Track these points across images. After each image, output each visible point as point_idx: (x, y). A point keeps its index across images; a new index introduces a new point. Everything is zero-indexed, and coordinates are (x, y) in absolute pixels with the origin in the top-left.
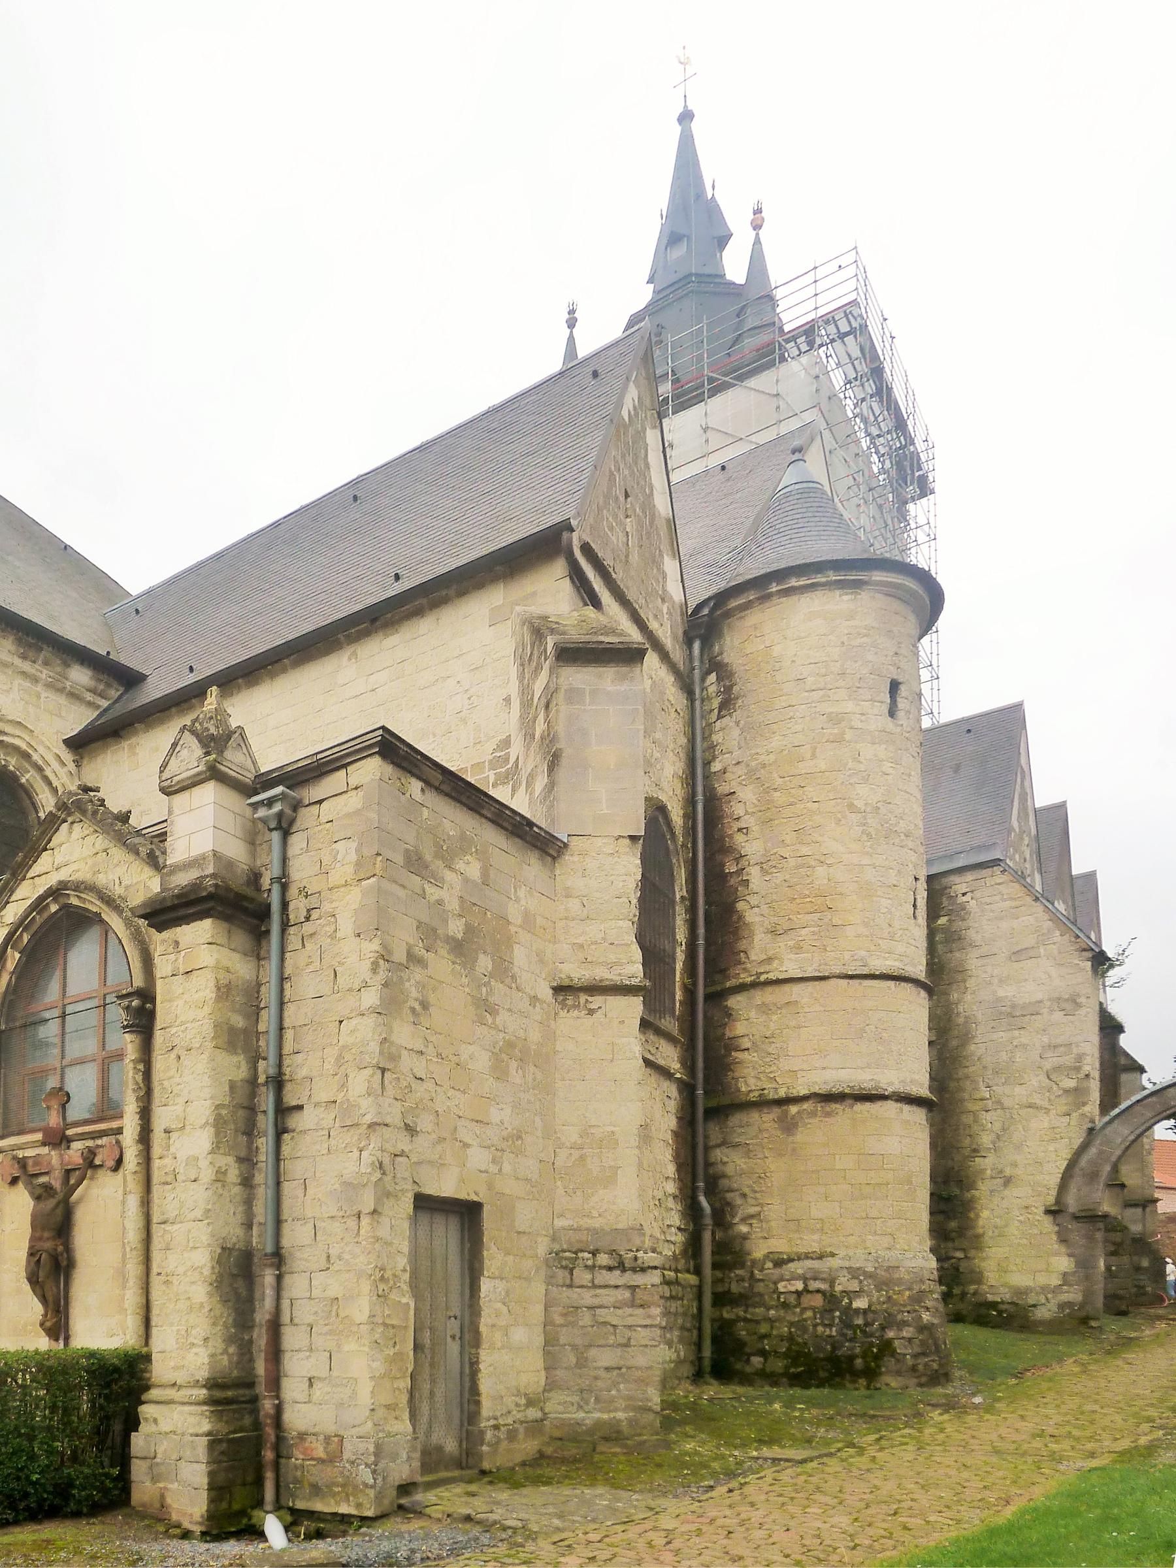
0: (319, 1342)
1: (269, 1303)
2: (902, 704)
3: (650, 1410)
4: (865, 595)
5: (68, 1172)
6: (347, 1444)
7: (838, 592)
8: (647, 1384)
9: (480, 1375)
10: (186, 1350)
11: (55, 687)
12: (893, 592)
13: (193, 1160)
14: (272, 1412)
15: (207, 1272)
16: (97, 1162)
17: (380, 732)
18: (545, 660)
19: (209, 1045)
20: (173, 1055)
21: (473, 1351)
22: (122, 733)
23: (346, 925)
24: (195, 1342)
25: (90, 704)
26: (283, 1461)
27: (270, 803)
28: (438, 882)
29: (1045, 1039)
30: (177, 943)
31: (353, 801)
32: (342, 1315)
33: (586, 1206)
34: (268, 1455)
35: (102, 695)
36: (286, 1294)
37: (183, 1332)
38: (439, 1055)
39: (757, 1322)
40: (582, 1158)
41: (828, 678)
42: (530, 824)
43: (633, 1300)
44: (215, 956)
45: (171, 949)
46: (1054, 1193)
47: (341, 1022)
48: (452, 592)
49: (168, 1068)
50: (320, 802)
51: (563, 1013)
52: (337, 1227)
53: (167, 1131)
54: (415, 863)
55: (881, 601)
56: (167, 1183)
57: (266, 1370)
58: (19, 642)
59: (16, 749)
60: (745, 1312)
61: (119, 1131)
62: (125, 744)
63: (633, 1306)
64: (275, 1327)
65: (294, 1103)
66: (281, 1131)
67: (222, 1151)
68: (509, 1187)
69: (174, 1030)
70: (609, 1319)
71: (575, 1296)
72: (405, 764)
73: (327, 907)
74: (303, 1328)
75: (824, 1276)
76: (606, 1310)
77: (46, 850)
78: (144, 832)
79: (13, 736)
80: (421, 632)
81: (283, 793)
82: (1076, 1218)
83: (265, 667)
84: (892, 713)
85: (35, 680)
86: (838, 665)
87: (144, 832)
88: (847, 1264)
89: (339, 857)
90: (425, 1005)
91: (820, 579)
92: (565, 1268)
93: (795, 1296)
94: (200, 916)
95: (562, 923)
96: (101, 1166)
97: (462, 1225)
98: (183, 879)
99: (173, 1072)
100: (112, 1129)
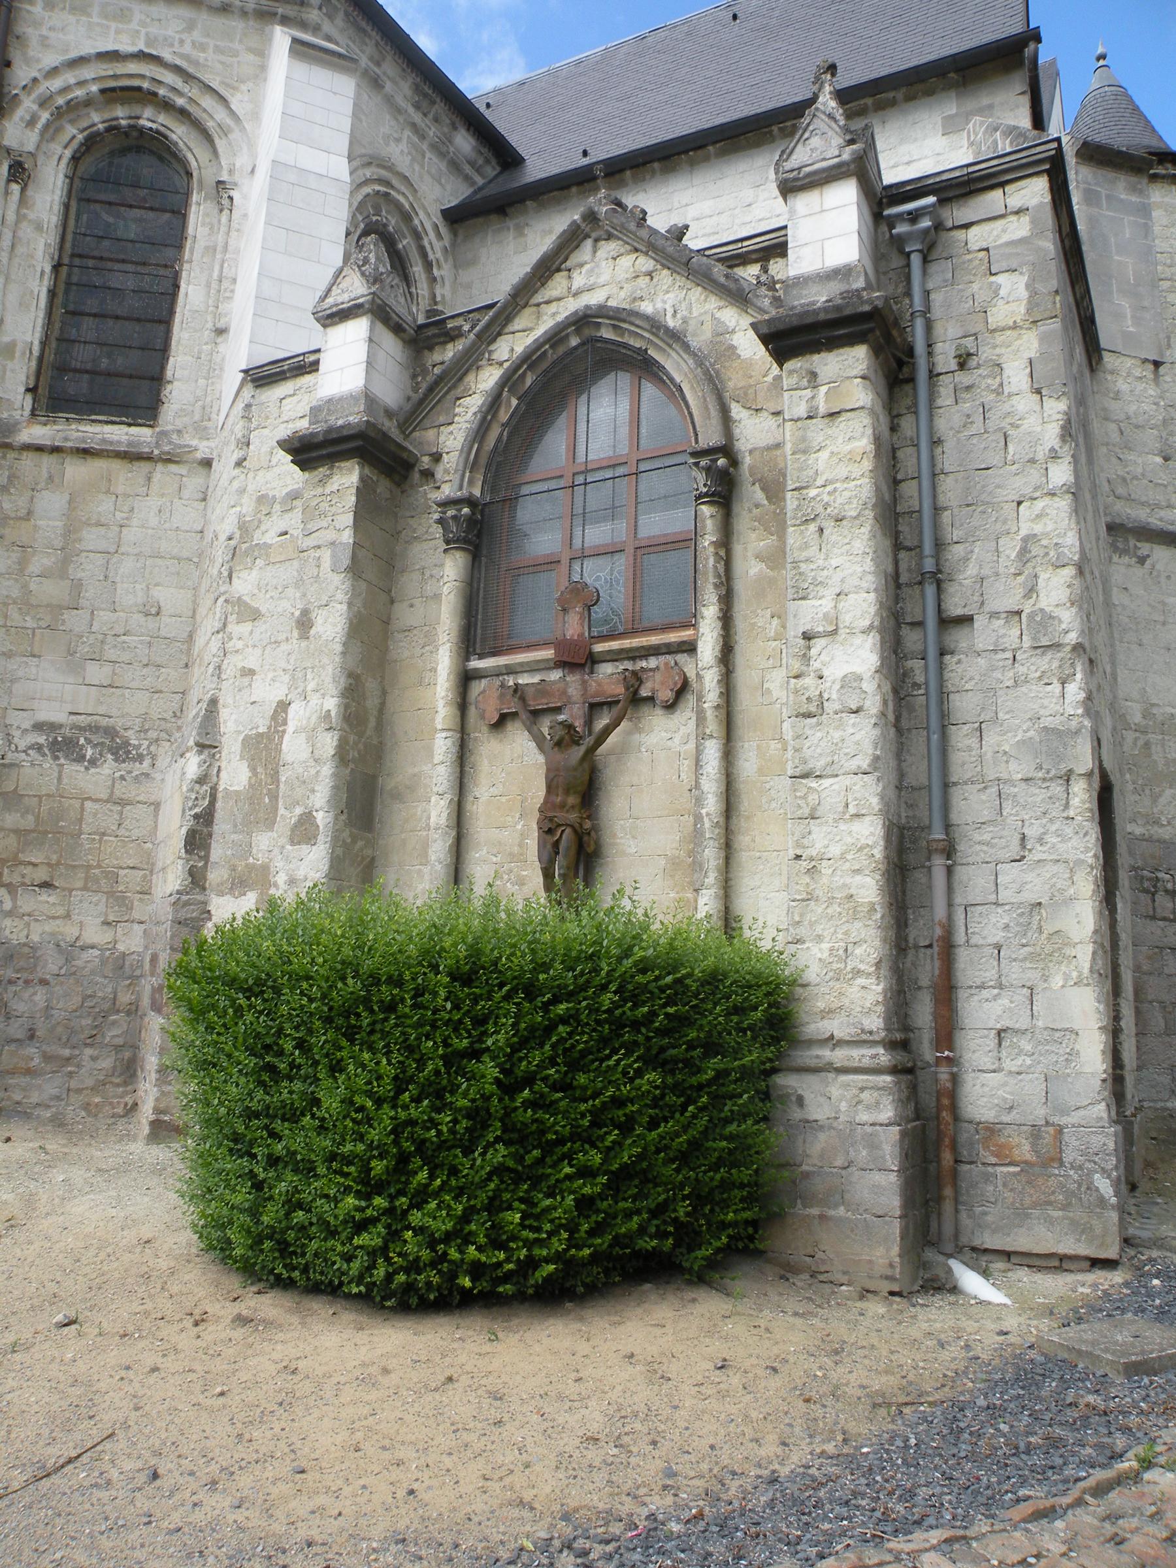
5: (594, 708)
6: (1068, 1136)
10: (840, 975)
11: (439, 149)
13: (850, 682)
15: (878, 852)
16: (644, 693)
19: (870, 514)
20: (813, 527)
22: (508, 210)
23: (1016, 376)
24: (862, 967)
25: (467, 178)
27: (914, 217)
30: (813, 375)
31: (1018, 228)
32: (1049, 928)
35: (478, 171)
36: (959, 899)
37: (841, 952)
40: (1147, 745)
45: (805, 382)
47: (1019, 503)
49: (806, 546)
50: (967, 226)
51: (1115, 558)
52: (1038, 795)
53: (808, 637)
56: (809, 715)
58: (416, 89)
59: (398, 206)
61: (690, 648)
62: (511, 224)
64: (947, 949)
65: (959, 612)
69: (812, 493)
71: (1159, 932)
73: (986, 353)
77: (558, 270)
79: (399, 192)
81: (933, 205)
83: (686, 152)
85: (423, 137)
89: (1002, 293)
92: (1146, 891)
96: (651, 699)
99: (812, 551)
100: (668, 645)
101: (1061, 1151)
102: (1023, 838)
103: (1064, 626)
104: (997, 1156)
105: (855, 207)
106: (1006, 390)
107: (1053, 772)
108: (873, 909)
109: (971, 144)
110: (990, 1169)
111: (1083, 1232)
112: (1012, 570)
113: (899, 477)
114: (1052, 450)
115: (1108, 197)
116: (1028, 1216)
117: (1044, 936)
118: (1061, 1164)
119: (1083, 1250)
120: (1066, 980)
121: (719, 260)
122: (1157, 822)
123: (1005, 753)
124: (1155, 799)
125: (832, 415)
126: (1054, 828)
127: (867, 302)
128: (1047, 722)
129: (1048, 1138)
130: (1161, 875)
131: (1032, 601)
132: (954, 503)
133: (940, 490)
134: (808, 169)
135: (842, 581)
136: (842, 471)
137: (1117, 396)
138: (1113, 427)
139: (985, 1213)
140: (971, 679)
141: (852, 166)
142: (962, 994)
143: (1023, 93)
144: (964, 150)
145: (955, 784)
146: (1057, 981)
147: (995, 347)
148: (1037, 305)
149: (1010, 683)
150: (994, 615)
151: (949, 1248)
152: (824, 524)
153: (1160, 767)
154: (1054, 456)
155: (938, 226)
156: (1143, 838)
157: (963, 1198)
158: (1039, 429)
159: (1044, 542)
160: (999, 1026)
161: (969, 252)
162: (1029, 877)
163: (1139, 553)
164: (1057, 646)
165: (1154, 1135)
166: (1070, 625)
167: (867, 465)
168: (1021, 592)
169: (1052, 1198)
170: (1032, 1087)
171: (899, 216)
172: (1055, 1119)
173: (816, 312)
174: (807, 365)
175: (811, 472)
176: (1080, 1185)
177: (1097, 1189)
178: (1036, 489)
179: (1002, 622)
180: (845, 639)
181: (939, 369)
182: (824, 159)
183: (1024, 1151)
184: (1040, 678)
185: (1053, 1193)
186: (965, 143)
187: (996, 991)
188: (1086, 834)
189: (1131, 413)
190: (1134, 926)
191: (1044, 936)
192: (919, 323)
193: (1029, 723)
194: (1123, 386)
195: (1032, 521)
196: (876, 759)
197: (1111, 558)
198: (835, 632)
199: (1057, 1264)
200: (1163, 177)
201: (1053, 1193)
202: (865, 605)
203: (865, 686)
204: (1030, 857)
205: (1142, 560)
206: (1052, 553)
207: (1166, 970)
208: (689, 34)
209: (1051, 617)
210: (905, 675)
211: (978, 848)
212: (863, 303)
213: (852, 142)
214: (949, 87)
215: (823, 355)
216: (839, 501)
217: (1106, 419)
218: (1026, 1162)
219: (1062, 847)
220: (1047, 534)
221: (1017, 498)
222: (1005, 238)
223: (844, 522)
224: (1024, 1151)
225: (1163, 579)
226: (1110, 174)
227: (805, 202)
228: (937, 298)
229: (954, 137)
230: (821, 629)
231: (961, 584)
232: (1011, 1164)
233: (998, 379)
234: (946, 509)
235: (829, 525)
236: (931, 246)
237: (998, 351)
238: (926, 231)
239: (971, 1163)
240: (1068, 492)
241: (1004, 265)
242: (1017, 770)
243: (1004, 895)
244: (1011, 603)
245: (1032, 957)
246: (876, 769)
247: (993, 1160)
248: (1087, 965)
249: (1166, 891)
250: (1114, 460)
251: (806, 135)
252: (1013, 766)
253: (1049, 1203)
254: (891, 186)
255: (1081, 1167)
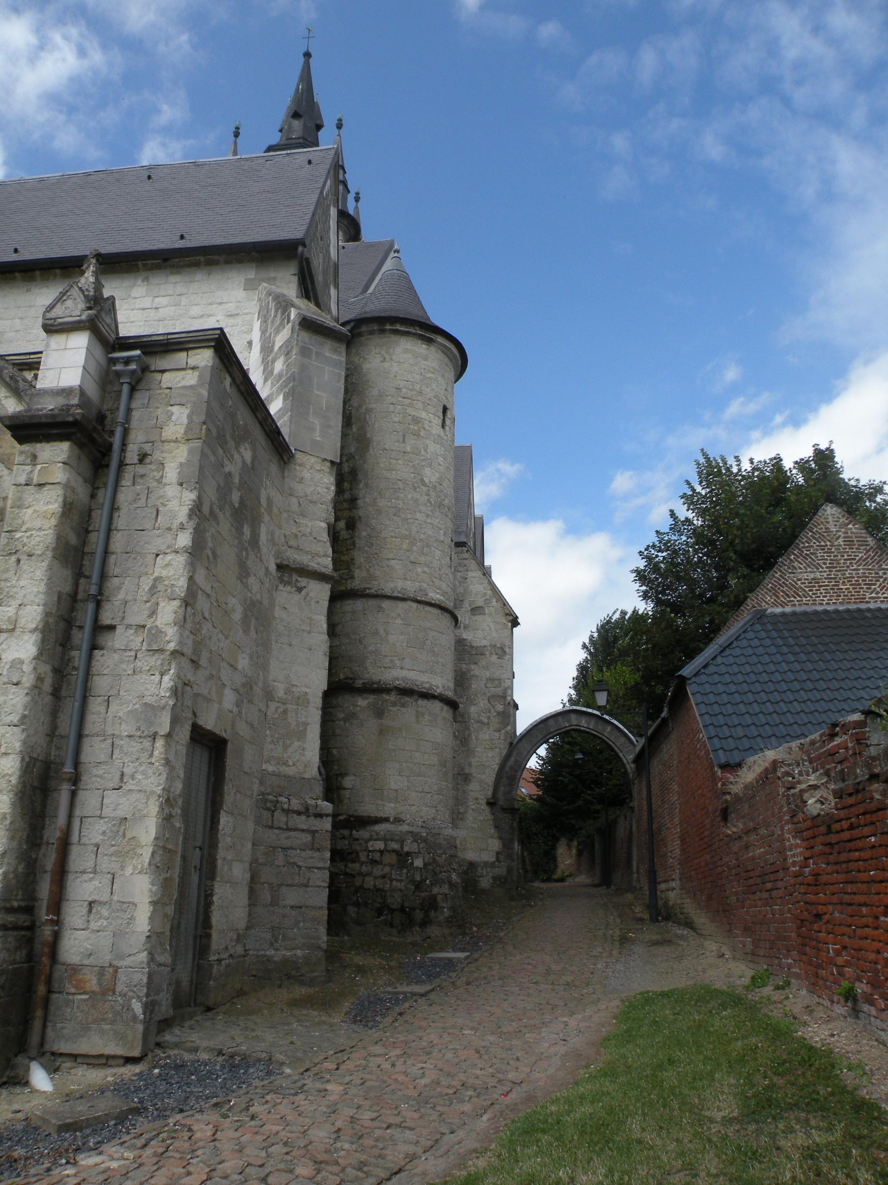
0: (105, 864)
1: (62, 820)
2: (448, 422)
3: (320, 948)
4: (433, 348)
6: (122, 976)
7: (420, 342)
8: (319, 923)
9: (213, 908)
12: (445, 351)
13: (17, 664)
14: (50, 939)
15: (14, 780)
17: (219, 332)
18: (288, 322)
19: (50, 554)
20: (13, 558)
21: (209, 883)
23: (171, 473)
26: (54, 996)
27: (127, 361)
28: (231, 459)
29: (488, 673)
30: (35, 457)
32: (129, 835)
33: (285, 755)
34: (42, 989)
36: (78, 812)
38: (217, 601)
39: (353, 876)
40: (285, 712)
41: (413, 393)
42: (279, 433)
43: (313, 844)
44: (67, 475)
45: (28, 461)
46: (491, 789)
47: (157, 555)
48: (222, 259)
50: (163, 371)
51: (281, 587)
52: (135, 747)
54: (221, 439)
55: (440, 355)
57: (51, 891)
60: (346, 866)
63: (312, 849)
64: (65, 845)
66: (94, 647)
67: (43, 658)
68: (243, 730)
70: (296, 860)
72: (225, 361)
73: (157, 456)
74: (91, 848)
75: (397, 838)
76: (294, 852)
78: (7, 358)
80: (197, 279)
81: (139, 356)
82: (504, 810)
84: (443, 426)
86: (419, 386)
87: (7, 358)
88: (411, 829)
89: (174, 418)
90: (215, 556)
91: (412, 330)
92: (268, 809)
93: (379, 854)
94: (60, 438)
95: (286, 515)
97: (210, 757)
98: (49, 405)
101: (115, 985)
102: (122, 775)
103: (167, 638)
104: (76, 987)
105: (84, 350)
106: (164, 481)
107: (146, 733)
108: (4, 818)
109: (259, 299)
110: (71, 997)
111: (121, 1039)
112: (145, 599)
113: (90, 529)
114: (182, 523)
115: (318, 354)
116: (89, 1029)
117: (126, 839)
118: (114, 993)
119: (120, 1051)
120: (134, 870)
121: (14, 364)
122: (286, 764)
123: (120, 717)
124: (286, 748)
125: (41, 485)
126: (141, 769)
127: (71, 415)
128: (148, 700)
129: (108, 976)
130: (280, 799)
131: (152, 620)
132: (119, 551)
133: (112, 540)
134: (60, 320)
135: (24, 596)
136: (38, 523)
137: (301, 480)
138: (295, 500)
139: (63, 1028)
140: (108, 667)
141: (87, 324)
142: (71, 877)
143: (295, 275)
144: (255, 302)
145: (87, 736)
146: (129, 870)
147: (162, 452)
148: (191, 429)
149: (130, 672)
150: (129, 626)
151: (33, 1052)
152: (21, 557)
153: (293, 727)
154: (182, 527)
155: (145, 369)
156: (274, 774)
157: (50, 1018)
158: (177, 509)
159: (166, 583)
160: (90, 899)
161: (161, 388)
162: (122, 800)
163: (299, 585)
164: (161, 651)
165: (254, 973)
166: (171, 637)
167: (54, 521)
168: (147, 613)
169: (105, 1016)
170: (105, 941)
171: (117, 359)
172: (115, 963)
173: (40, 416)
174: (32, 450)
175: (19, 521)
176: (123, 1007)
177: (133, 1010)
178: (168, 547)
179: (133, 631)
180: (19, 635)
181: (128, 461)
182: (71, 316)
183: (93, 984)
184: (149, 670)
185: (107, 1012)
186: (256, 298)
187: (92, 875)
188: (160, 775)
189: (309, 493)
190: (255, 832)
191: (126, 839)
192: (119, 431)
193: (137, 699)
194: (307, 475)
195: (162, 568)
196: (24, 717)
197: (277, 587)
198: (13, 630)
199: (104, 1061)
200: (414, 334)
201: (107, 1012)
202: (35, 614)
203: (25, 668)
204: (126, 787)
205: (300, 590)
206: (169, 590)
207: (277, 863)
208: (118, 180)
209: (161, 632)
210: (69, 660)
211: (94, 779)
212: (69, 415)
213: (89, 308)
214: (252, 260)
215: (44, 444)
216: (32, 543)
217: (291, 495)
218: (93, 992)
219: (145, 782)
220: (169, 577)
221: (155, 552)
222: (183, 383)
223: (33, 558)
224: (93, 984)
225: (313, 603)
226: (320, 339)
227: (57, 341)
228: (136, 415)
229: (250, 292)
230: (5, 627)
231: (113, 604)
232: (84, 993)
233: (161, 473)
234: (113, 553)
235: (23, 558)
236: (138, 381)
237: (164, 455)
238: (133, 372)
239: (60, 992)
240: (186, 552)
241: (178, 401)
242: (126, 729)
243: (106, 811)
244: (139, 619)
245: (116, 854)
246: (23, 724)
247: (73, 990)
248: (147, 860)
249: (283, 810)
250: (292, 522)
251: (65, 298)
252: (123, 727)
253: (103, 1020)
254: (122, 338)
255: (125, 995)
